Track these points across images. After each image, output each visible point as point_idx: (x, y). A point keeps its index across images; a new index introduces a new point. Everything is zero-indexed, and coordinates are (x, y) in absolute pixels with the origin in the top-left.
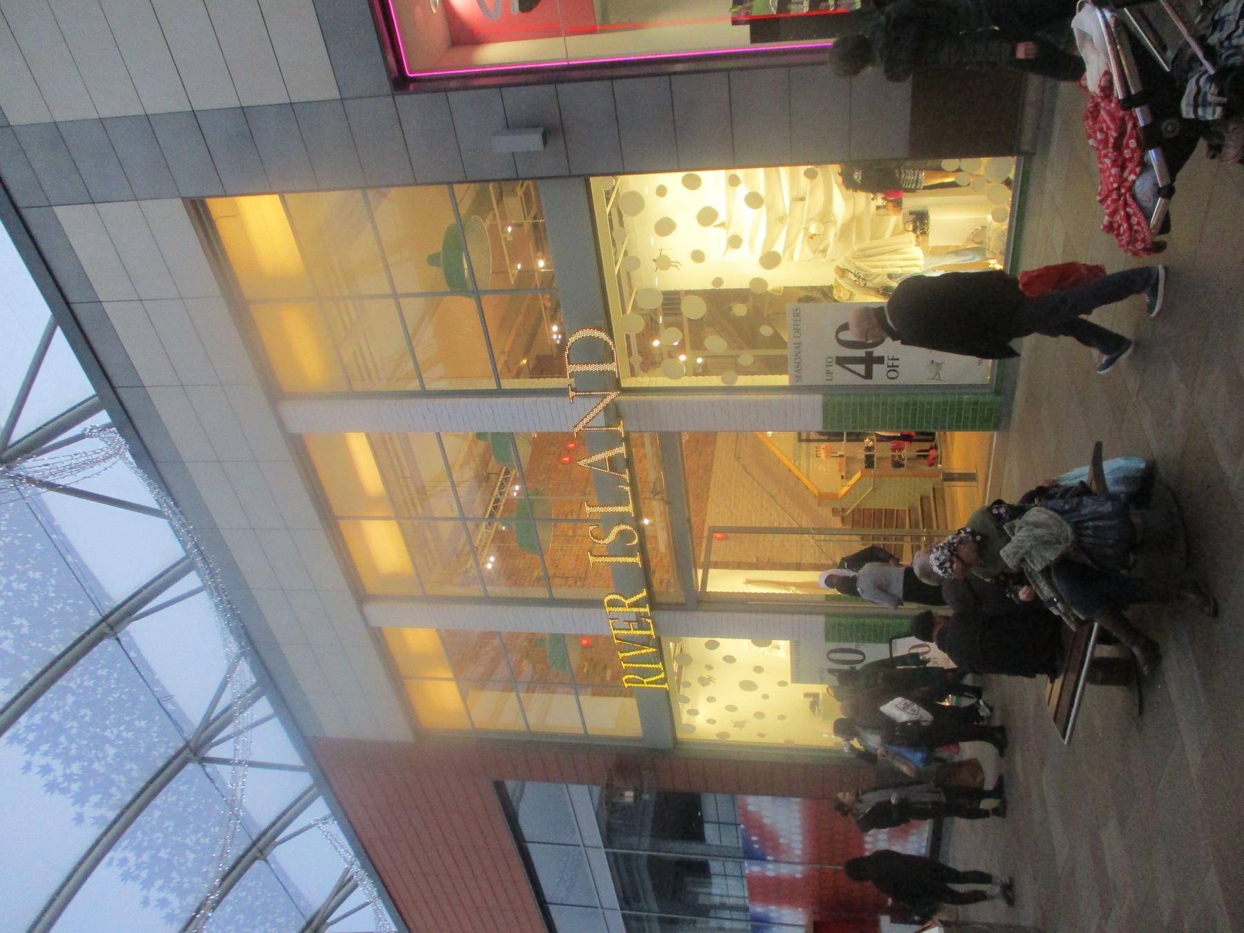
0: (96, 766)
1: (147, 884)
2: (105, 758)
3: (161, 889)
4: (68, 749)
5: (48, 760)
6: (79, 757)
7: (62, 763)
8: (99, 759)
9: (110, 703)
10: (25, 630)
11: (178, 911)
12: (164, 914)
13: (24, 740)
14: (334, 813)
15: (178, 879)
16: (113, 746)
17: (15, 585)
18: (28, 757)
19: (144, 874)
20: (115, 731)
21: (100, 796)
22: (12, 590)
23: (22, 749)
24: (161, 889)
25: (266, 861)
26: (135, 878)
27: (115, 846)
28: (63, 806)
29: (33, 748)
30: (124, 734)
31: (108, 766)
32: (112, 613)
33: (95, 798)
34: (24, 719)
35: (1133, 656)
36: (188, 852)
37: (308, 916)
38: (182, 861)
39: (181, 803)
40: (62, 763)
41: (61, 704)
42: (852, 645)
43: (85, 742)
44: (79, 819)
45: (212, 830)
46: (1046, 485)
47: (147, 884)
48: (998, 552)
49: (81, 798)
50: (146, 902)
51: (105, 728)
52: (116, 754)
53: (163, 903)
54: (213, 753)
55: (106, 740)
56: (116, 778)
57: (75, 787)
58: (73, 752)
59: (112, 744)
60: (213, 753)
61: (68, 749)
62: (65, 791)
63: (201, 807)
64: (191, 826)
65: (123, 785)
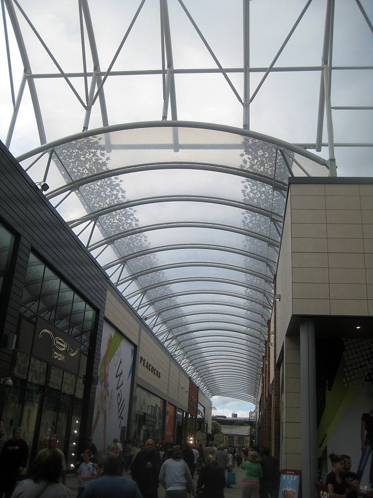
4: (254, 190)
6: (127, 223)
9: (73, 159)
10: (82, 157)
14: (25, 172)
16: (264, 168)
18: (99, 141)
22: (83, 168)
23: (135, 216)
28: (123, 186)
35: (57, 453)
36: (88, 168)
44: (121, 181)
46: (184, 472)
49: (118, 185)
53: (245, 162)
57: (132, 217)
58: (92, 154)
59: (86, 168)
62: (121, 189)
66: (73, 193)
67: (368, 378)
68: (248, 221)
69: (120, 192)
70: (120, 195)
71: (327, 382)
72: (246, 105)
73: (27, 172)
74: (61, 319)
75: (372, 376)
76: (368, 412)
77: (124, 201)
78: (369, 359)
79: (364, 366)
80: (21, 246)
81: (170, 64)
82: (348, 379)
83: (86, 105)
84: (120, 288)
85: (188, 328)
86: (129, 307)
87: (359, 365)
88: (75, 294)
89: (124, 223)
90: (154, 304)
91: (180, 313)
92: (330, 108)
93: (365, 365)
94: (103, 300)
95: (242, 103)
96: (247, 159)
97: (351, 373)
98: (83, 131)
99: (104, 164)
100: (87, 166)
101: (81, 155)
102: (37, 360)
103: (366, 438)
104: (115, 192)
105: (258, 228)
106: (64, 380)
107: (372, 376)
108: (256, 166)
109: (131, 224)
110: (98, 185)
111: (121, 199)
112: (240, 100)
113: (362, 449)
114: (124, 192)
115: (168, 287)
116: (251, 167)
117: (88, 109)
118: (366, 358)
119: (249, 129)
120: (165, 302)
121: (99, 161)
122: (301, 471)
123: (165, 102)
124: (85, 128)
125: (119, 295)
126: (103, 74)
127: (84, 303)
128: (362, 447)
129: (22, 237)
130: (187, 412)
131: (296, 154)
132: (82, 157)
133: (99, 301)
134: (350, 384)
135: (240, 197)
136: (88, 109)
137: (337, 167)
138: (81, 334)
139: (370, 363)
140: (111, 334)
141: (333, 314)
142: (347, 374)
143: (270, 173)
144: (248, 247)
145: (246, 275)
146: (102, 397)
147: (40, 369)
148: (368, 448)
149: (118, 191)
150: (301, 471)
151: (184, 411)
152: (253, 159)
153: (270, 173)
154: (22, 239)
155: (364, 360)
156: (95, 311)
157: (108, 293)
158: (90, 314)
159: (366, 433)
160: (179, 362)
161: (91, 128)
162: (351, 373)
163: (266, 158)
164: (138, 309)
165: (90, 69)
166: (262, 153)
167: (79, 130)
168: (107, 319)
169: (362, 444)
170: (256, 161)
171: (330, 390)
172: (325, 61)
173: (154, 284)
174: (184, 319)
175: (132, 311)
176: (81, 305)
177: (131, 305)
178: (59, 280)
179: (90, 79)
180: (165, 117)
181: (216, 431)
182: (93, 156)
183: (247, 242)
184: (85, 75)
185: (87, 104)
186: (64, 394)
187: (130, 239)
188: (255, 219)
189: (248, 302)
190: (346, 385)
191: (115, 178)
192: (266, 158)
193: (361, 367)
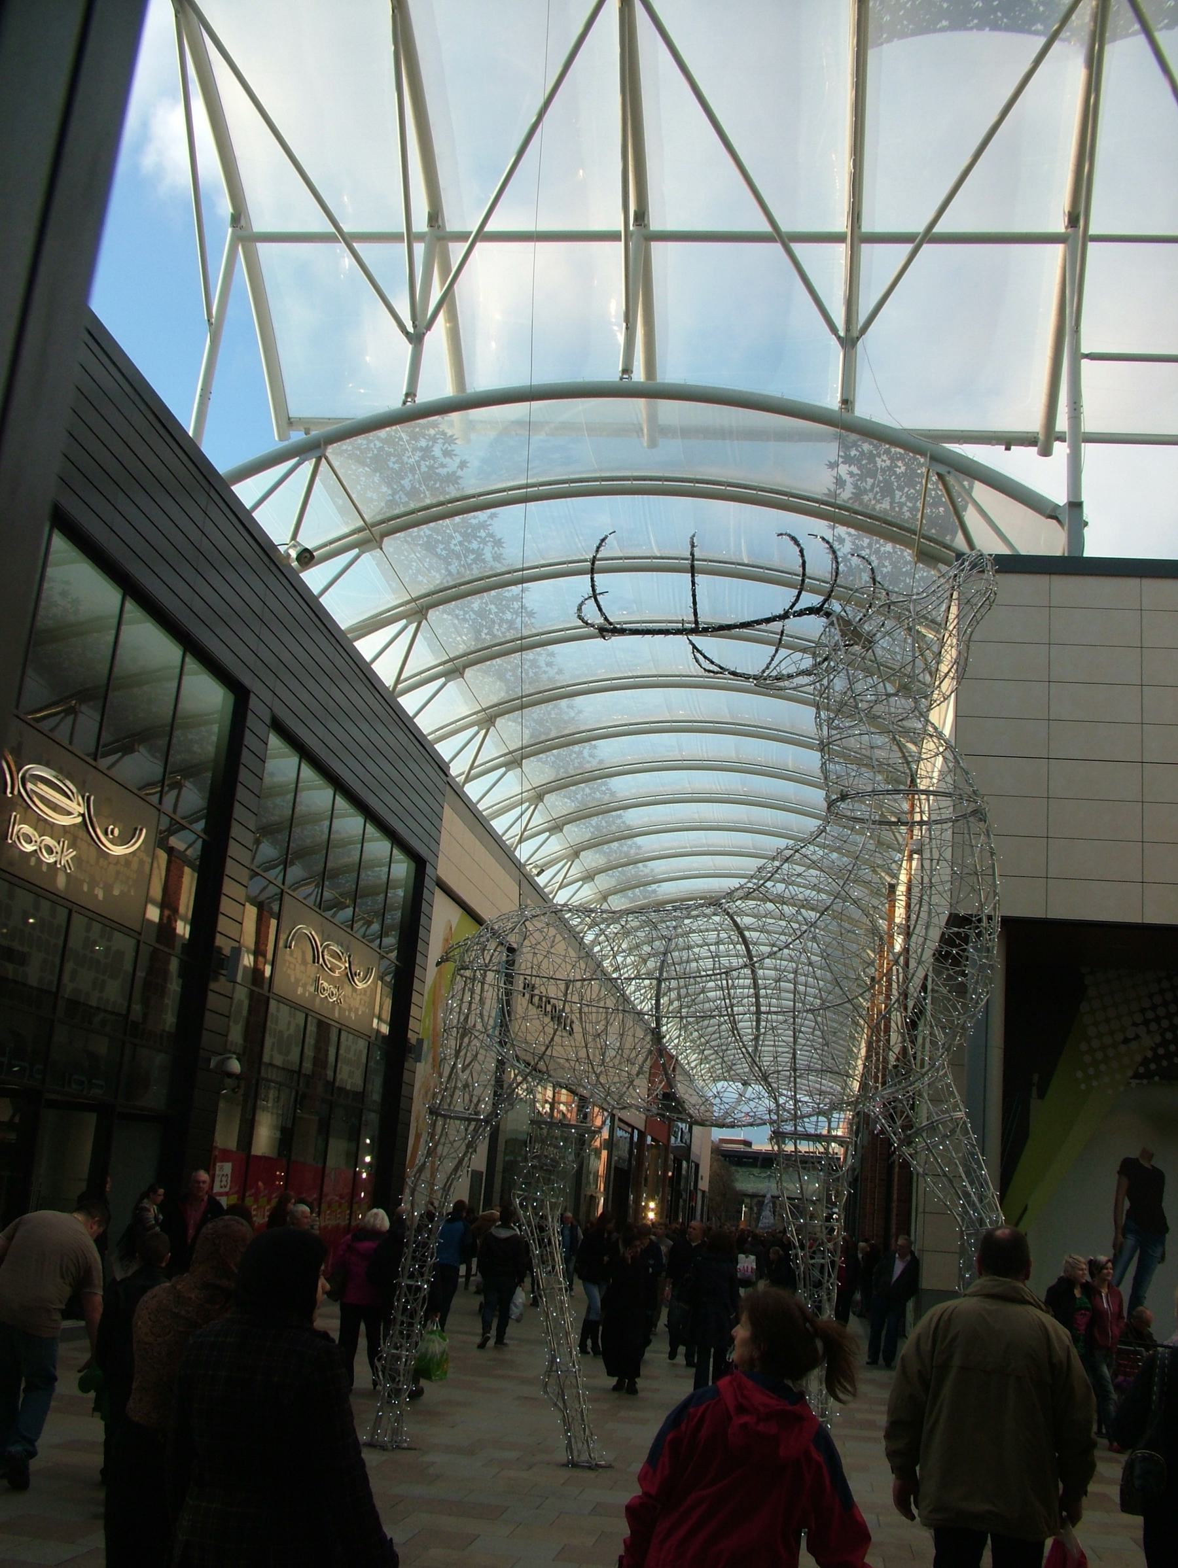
2: (878, 502)
5: (849, 480)
7: (853, 493)
16: (891, 504)
20: (903, 499)
24: (851, 474)
29: (848, 460)
30: (905, 509)
38: (878, 497)
40: (853, 493)
42: (75, 790)
43: (881, 478)
48: (1045, 1539)
51: (900, 489)
53: (840, 482)
57: (483, 534)
58: (419, 454)
62: (491, 535)
64: (912, 491)
66: (366, 557)
67: (1141, 1070)
69: (489, 544)
70: (488, 554)
71: (1036, 1077)
72: (849, 342)
73: (415, 720)
74: (128, 749)
75: (1177, 1060)
76: (1134, 1154)
77: (500, 568)
78: (1146, 1023)
79: (1134, 1039)
80: (251, 721)
81: (641, 216)
82: (1091, 1071)
83: (411, 329)
84: (473, 791)
85: (654, 891)
86: (494, 840)
87: (1119, 1037)
88: (303, 765)
89: (493, 622)
90: (462, 675)
91: (606, 798)
92: (1078, 356)
93: (1137, 1037)
94: (433, 832)
95: (839, 338)
96: (845, 477)
97: (1099, 1055)
98: (404, 403)
99: (452, 479)
100: (406, 483)
102: (282, 1005)
103: (1127, 1218)
104: (475, 545)
105: (883, 497)
106: (341, 1052)
107: (1177, 1060)
108: (871, 495)
109: (511, 623)
112: (833, 329)
113: (1114, 1246)
114: (498, 543)
115: (483, 526)
117: (416, 339)
118: (1138, 1018)
119: (853, 411)
120: (476, 606)
121: (439, 471)
123: (627, 328)
124: (411, 394)
125: (469, 809)
126: (461, 237)
127: (329, 792)
128: (1116, 1238)
129: (252, 694)
130: (643, 1130)
131: (977, 485)
133: (426, 839)
134: (1095, 1083)
136: (416, 339)
137: (1086, 524)
138: (286, 863)
139: (1149, 1032)
140: (449, 921)
141: (1052, 915)
142: (1087, 1059)
143: (908, 514)
146: (426, 1093)
147: (288, 1029)
148: (1130, 1241)
151: (633, 1128)
152: (862, 478)
153: (908, 514)
154: (253, 702)
155: (1135, 1024)
156: (413, 865)
157: (448, 813)
158: (401, 869)
159: (1127, 1204)
160: (551, 896)
161: (425, 395)
162: (1099, 1055)
163: (898, 477)
164: (467, 780)
165: (421, 224)
166: (888, 463)
167: (393, 401)
168: (445, 883)
169: (1116, 1233)
171: (1041, 1096)
172: (1073, 220)
173: (565, 775)
174: (571, 707)
175: (503, 851)
176: (379, 847)
177: (368, 658)
178: (296, 759)
179: (419, 249)
180: (627, 370)
181: (722, 1183)
182: (423, 458)
183: (450, 470)
184: (411, 237)
185: (415, 326)
186: (341, 1089)
187: (389, 441)
190: (1083, 1087)
191: (644, 866)
192: (898, 477)
193: (1126, 1041)
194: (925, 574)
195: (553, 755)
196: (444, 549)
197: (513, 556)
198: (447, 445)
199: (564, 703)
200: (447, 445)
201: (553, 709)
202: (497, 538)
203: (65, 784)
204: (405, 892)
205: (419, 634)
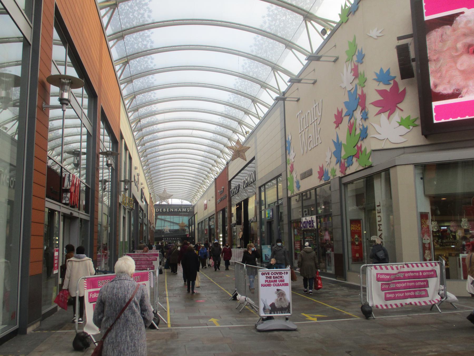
0: (278, 16)
1: (269, 15)
3: (269, 20)
4: (242, 85)
8: (280, 16)
9: (123, 16)
10: (281, 26)
11: (271, 9)
12: (269, 6)
13: (269, 12)
15: (243, 84)
16: (286, 18)
17: (261, 72)
19: (271, 13)
21: (271, 19)
24: (269, 20)
25: (285, 48)
26: (269, 11)
27: (249, 59)
31: (280, 19)
32: (266, 84)
33: (257, 48)
34: (228, 107)
36: (257, 69)
37: (311, 11)
39: (277, 46)
41: (282, 16)
45: (264, 73)
47: (269, 15)
50: (264, 17)
51: (248, 89)
52: (283, 20)
53: (230, 98)
54: (309, 24)
55: (286, 16)
56: (278, 21)
59: (286, 18)
60: (309, 24)
61: (242, 85)
62: (150, 40)
63: (278, 52)
65: (276, 24)
68: (247, 65)
70: (146, 15)
89: (142, 65)
101: (130, 12)
109: (146, 45)
110: (133, 37)
111: (147, 19)
114: (150, 11)
116: (233, 101)
121: (149, 67)
122: (89, 292)
132: (270, 46)
135: (240, 70)
144: (267, 25)
145: (225, 107)
149: (148, 42)
150: (89, 292)
152: (148, 81)
170: (260, 51)
188: (244, 84)
189: (203, 158)
194: (295, 27)
195: (137, 61)
196: (132, 15)
197: (156, 83)
198: (149, 13)
199: (150, 76)
200: (149, 13)
201: (150, 107)
202: (150, 9)
203: (77, 203)
204: (49, 57)
205: (122, 75)
